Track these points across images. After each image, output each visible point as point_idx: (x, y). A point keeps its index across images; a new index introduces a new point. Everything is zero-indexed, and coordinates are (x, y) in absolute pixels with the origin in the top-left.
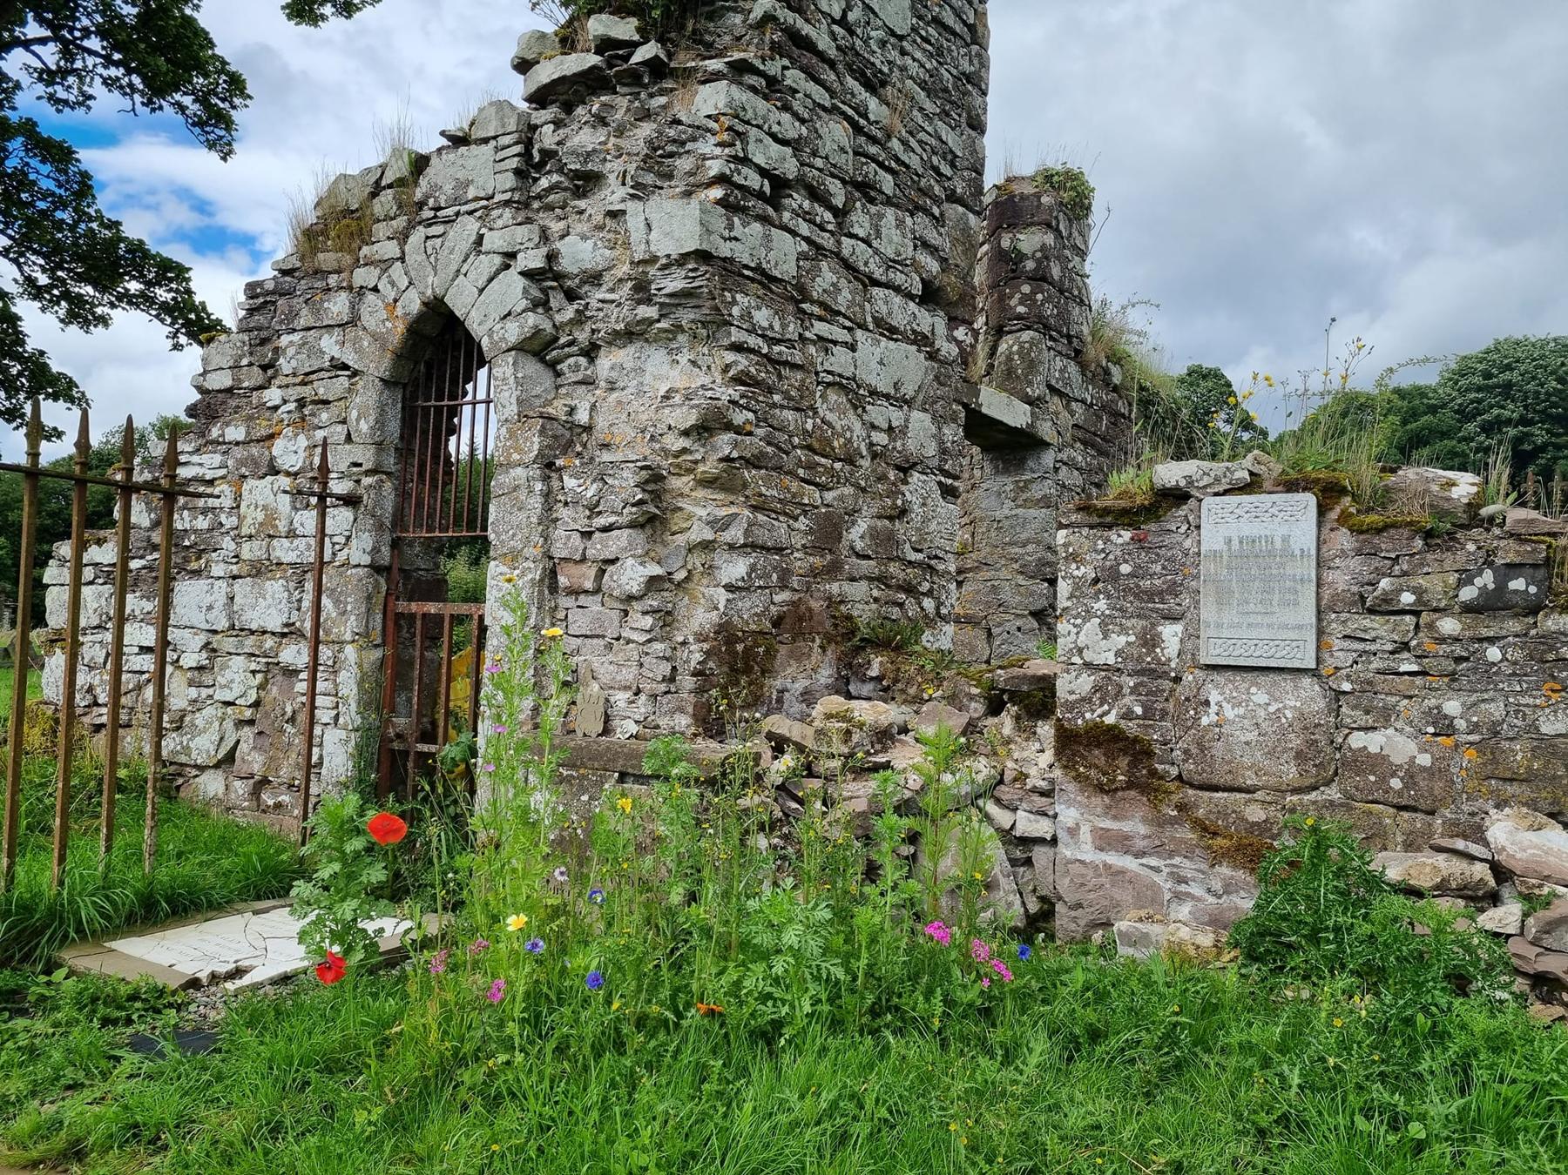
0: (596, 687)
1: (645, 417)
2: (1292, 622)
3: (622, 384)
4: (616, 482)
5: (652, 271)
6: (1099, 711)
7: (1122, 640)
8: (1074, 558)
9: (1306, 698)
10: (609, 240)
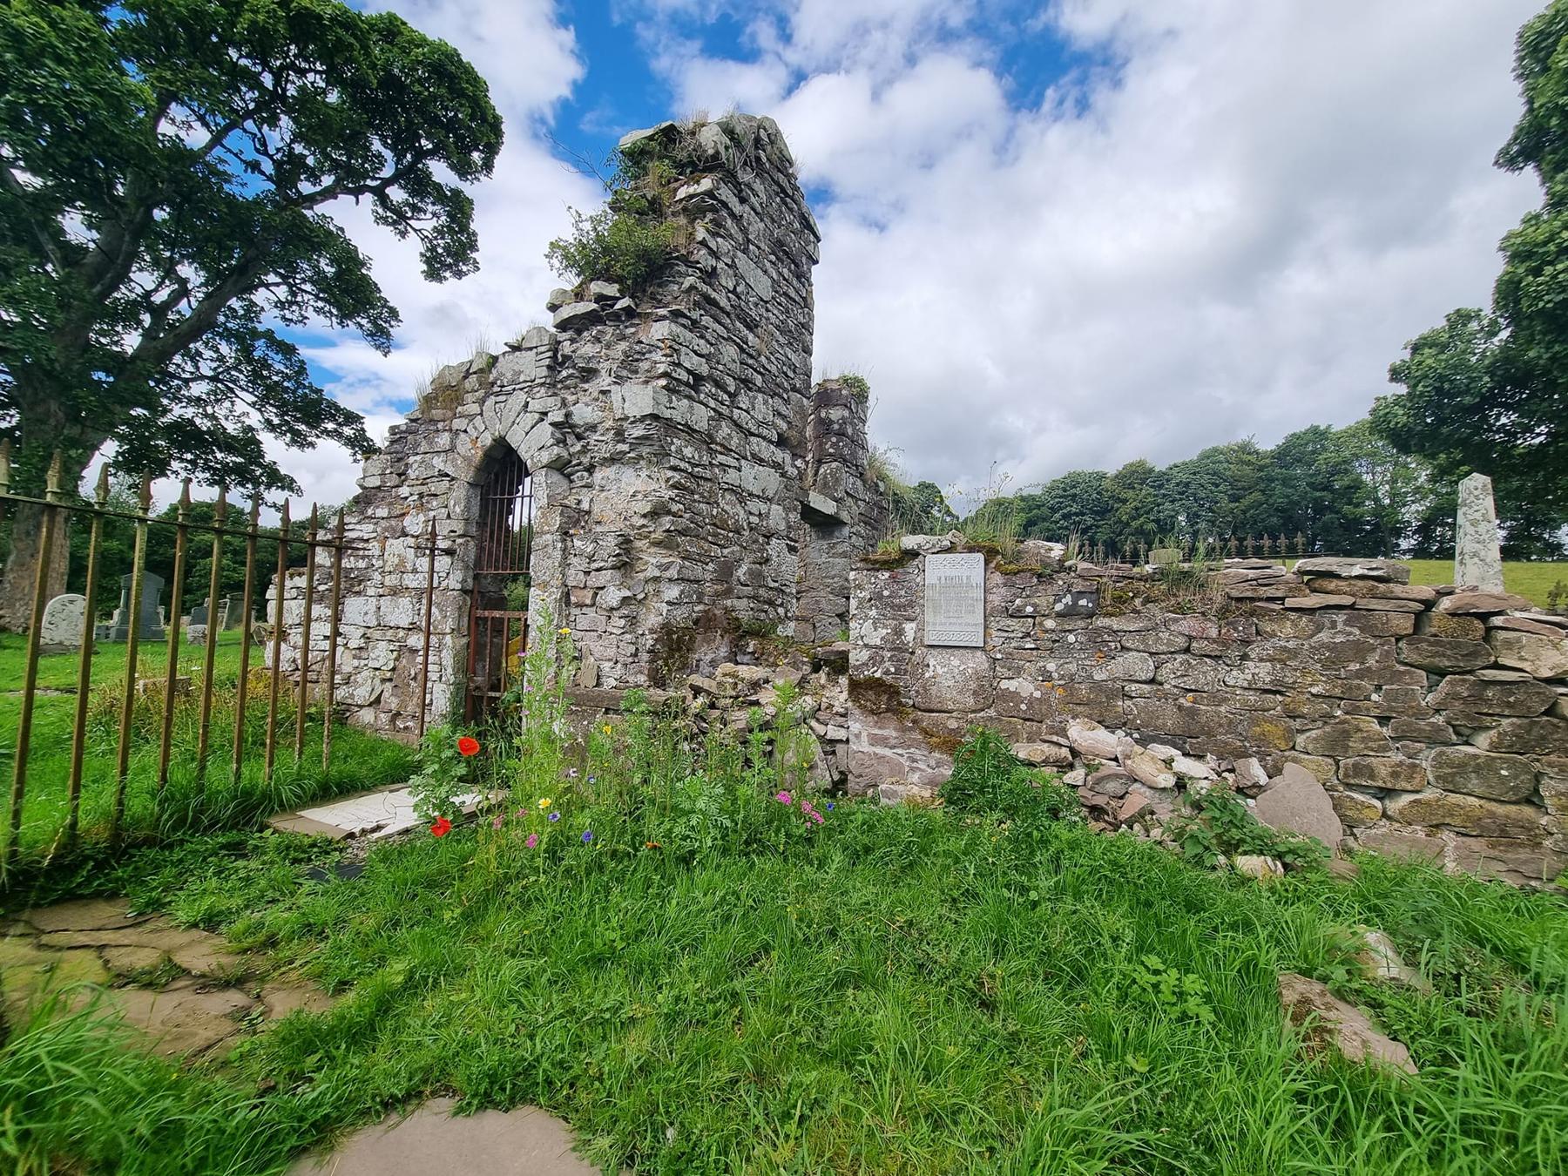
8: (859, 587)
9: (979, 662)
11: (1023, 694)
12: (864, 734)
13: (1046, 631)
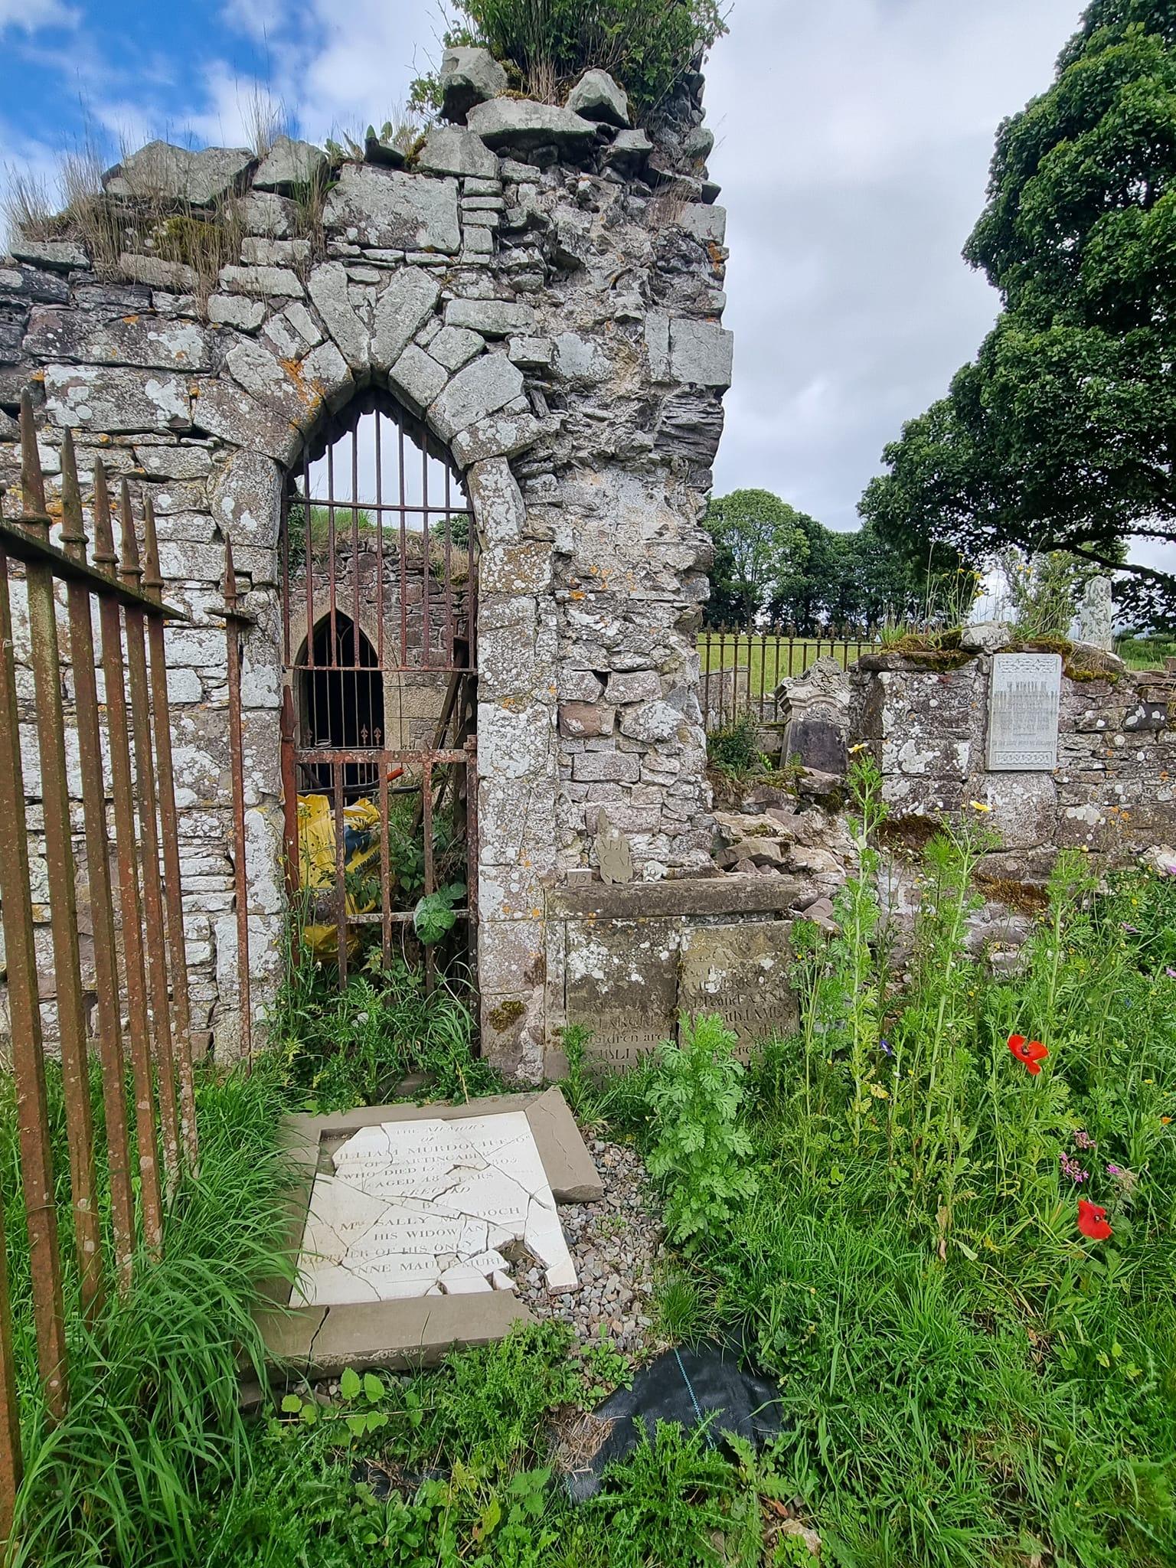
0: (616, 833)
1: (636, 553)
2: (1045, 740)
3: (602, 514)
4: (645, 622)
5: (668, 396)
6: (912, 807)
7: (930, 755)
8: (896, 695)
9: (1043, 789)
10: (611, 349)
11: (1090, 823)
12: (901, 891)
13: (1116, 749)
